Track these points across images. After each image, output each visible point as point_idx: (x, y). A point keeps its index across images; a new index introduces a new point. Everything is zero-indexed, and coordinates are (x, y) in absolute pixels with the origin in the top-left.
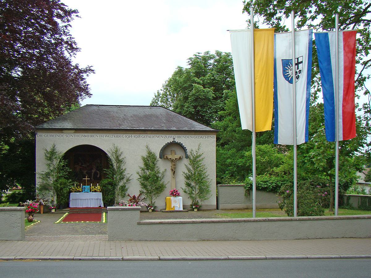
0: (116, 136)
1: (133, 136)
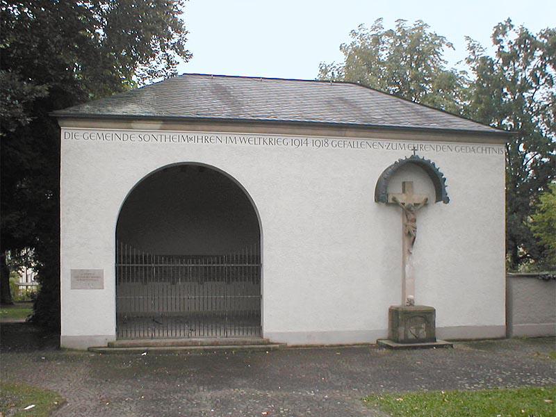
0: (268, 141)
1: (310, 140)
